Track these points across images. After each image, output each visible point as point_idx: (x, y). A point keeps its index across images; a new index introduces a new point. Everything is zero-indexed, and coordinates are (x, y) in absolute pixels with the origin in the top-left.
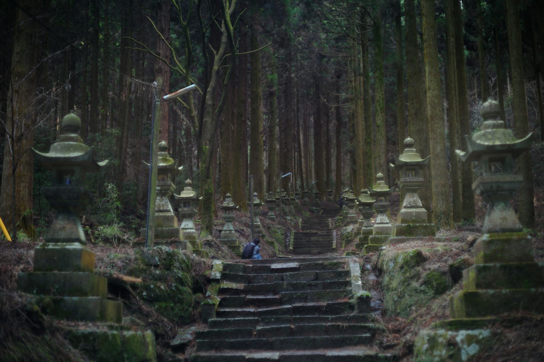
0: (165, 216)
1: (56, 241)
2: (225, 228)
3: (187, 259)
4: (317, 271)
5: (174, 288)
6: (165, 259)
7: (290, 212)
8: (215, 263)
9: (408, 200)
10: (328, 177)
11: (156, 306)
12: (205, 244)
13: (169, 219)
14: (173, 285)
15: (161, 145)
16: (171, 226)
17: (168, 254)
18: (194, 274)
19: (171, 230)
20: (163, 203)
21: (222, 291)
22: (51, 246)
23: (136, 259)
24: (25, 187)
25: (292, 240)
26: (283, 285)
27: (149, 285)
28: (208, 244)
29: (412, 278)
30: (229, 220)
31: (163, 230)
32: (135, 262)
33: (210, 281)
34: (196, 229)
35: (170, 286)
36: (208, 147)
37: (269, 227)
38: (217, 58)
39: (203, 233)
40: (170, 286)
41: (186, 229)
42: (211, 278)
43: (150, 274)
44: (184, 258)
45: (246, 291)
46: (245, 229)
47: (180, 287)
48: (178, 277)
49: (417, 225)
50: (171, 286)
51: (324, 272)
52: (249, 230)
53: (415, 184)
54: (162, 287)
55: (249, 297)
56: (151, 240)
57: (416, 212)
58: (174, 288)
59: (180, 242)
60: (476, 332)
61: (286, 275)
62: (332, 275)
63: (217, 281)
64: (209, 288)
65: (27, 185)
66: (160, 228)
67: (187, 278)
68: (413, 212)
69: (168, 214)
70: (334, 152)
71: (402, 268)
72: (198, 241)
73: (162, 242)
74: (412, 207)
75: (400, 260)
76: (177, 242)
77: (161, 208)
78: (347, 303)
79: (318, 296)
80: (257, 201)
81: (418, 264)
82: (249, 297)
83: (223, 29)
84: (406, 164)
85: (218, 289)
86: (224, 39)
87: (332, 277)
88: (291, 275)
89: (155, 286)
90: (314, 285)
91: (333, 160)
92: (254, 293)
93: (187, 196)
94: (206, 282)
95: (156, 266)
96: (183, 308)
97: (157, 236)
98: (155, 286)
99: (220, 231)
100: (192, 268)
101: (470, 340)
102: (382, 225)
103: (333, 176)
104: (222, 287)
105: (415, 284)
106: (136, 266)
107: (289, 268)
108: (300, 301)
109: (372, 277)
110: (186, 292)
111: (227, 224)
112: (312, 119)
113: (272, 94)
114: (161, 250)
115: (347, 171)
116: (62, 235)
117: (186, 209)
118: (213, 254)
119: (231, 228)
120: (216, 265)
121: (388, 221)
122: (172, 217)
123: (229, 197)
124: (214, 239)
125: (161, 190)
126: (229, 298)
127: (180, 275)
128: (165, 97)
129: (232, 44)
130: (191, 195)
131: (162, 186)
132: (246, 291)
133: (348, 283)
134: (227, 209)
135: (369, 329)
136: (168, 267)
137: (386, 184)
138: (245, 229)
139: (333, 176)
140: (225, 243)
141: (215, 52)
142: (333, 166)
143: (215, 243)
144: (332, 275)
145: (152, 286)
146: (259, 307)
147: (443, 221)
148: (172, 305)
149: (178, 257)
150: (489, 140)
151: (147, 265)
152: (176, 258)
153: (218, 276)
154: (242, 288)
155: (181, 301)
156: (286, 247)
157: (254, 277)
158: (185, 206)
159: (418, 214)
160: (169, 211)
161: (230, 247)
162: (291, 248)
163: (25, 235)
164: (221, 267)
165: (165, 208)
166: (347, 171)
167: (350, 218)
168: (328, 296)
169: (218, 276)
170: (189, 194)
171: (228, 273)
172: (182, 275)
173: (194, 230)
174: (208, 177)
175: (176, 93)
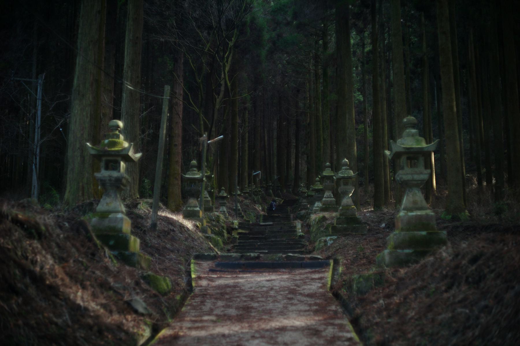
1: (191, 207)
9: (327, 194)
17: (218, 216)
21: (239, 234)
22: (189, 209)
29: (321, 227)
31: (117, 218)
33: (234, 229)
35: (219, 229)
36: (212, 158)
38: (218, 100)
45: (249, 234)
60: (333, 237)
63: (236, 229)
64: (233, 232)
70: (293, 151)
71: (317, 223)
75: (317, 220)
81: (324, 221)
83: (223, 82)
84: (326, 176)
86: (223, 88)
91: (293, 156)
95: (214, 221)
101: (331, 239)
103: (292, 172)
105: (322, 229)
109: (306, 229)
112: (275, 123)
113: (245, 109)
115: (303, 167)
116: (193, 205)
123: (223, 190)
133: (295, 231)
135: (302, 245)
139: (292, 172)
141: (216, 97)
142: (293, 162)
150: (343, 174)
153: (237, 227)
159: (331, 201)
166: (303, 167)
169: (237, 227)
171: (241, 226)
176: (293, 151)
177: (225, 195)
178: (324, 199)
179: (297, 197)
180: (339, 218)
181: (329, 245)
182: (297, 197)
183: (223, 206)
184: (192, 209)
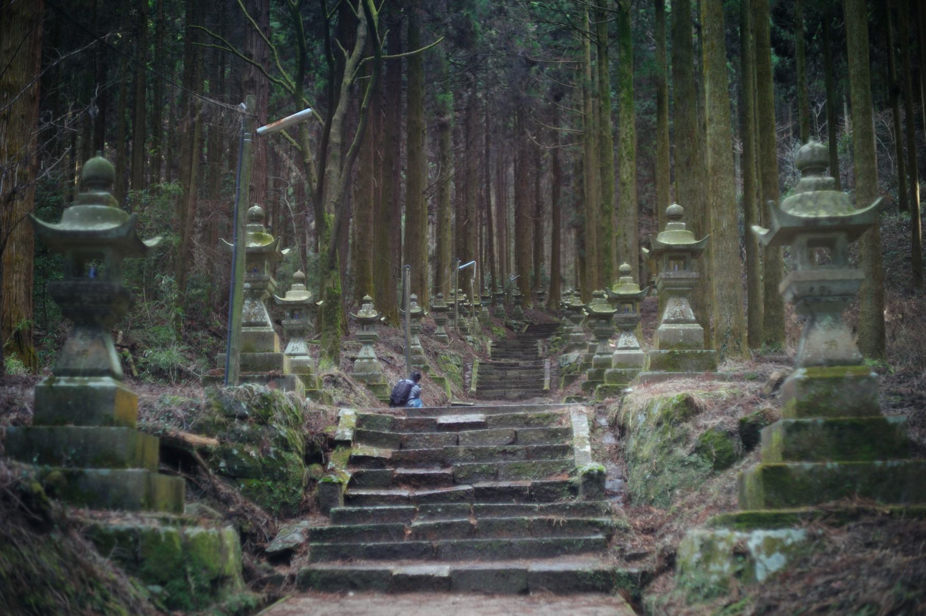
0: (259, 334)
1: (72, 373)
2: (362, 354)
3: (296, 405)
5: (272, 456)
6: (258, 407)
8: (343, 413)
11: (243, 486)
12: (328, 381)
13: (266, 338)
14: (272, 449)
15: (252, 211)
17: (264, 398)
19: (269, 356)
21: (355, 461)
22: (63, 382)
23: (209, 406)
25: (475, 376)
28: (333, 381)
29: (676, 441)
30: (368, 341)
31: (254, 357)
32: (207, 411)
33: (333, 443)
34: (312, 356)
37: (436, 354)
38: (349, 63)
39: (324, 363)
40: (265, 452)
41: (295, 355)
42: (336, 438)
43: (233, 431)
44: (291, 404)
45: (395, 462)
47: (284, 454)
48: (280, 436)
49: (687, 351)
50: (268, 452)
51: (528, 431)
55: (401, 471)
57: (684, 330)
58: (272, 456)
59: (284, 377)
60: (780, 534)
61: (463, 435)
62: (542, 435)
63: (347, 444)
64: (333, 455)
66: (249, 354)
69: (264, 330)
70: (548, 227)
71: (659, 424)
74: (677, 322)
75: (657, 412)
76: (278, 377)
77: (253, 320)
78: (565, 483)
79: (516, 470)
81: (686, 417)
82: (401, 471)
83: (360, 14)
84: (669, 249)
86: (362, 31)
87: (541, 438)
88: (472, 435)
89: (241, 451)
95: (243, 418)
97: (244, 367)
98: (241, 451)
99: (353, 359)
101: (771, 546)
102: (627, 352)
103: (546, 268)
104: (354, 454)
105: (681, 452)
106: (208, 418)
109: (609, 440)
110: (293, 463)
113: (443, 127)
114: (251, 390)
117: (294, 321)
118: (340, 398)
120: (345, 417)
123: (368, 301)
124: (343, 373)
125: (252, 289)
126: (366, 473)
127: (282, 434)
130: (304, 298)
131: (254, 282)
135: (602, 527)
138: (395, 355)
139: (546, 268)
140: (360, 379)
141: (346, 54)
142: (547, 250)
143: (344, 379)
144: (542, 435)
145: (235, 452)
146: (417, 488)
148: (269, 483)
150: (808, 209)
151: (227, 416)
152: (277, 404)
153: (349, 435)
154: (389, 456)
157: (409, 439)
158: (292, 316)
160: (265, 324)
161: (369, 387)
162: (473, 389)
163: (18, 362)
165: (258, 320)
167: (574, 339)
168: (534, 471)
169: (349, 435)
170: (300, 295)
173: (307, 358)
174: (332, 268)
176: (548, 227)
177: (373, 315)
178: (663, 327)
179: (556, 319)
180: (797, 427)
181: (761, 576)
182: (556, 319)
183: (366, 343)
184: (76, 382)
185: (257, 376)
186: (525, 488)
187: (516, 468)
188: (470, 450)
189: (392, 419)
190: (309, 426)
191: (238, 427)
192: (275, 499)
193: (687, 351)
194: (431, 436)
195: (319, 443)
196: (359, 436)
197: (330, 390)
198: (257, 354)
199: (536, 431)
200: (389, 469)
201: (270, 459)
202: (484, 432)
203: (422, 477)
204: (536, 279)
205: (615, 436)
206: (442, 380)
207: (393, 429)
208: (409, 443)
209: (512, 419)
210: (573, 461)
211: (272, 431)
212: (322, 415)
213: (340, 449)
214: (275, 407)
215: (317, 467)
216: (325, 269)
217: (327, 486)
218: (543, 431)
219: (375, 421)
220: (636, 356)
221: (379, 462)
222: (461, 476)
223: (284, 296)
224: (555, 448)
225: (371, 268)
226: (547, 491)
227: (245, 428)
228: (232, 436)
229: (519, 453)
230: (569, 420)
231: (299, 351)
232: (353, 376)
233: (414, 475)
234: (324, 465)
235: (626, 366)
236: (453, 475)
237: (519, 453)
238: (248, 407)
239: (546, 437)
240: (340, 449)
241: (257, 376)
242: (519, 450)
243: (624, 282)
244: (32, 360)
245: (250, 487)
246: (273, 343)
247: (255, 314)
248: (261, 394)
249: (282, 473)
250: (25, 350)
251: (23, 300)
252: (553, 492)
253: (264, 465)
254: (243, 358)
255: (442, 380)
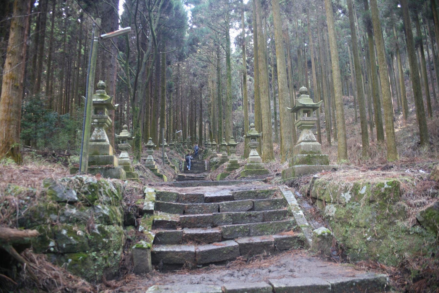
0: (102, 145)
2: (148, 158)
3: (117, 189)
4: (254, 200)
5: (97, 232)
6: (86, 193)
7: (179, 151)
8: (147, 191)
10: (195, 135)
11: (70, 260)
12: (136, 168)
13: (106, 148)
14: (96, 226)
15: (100, 84)
16: (106, 154)
17: (91, 186)
18: (125, 204)
19: (107, 157)
20: (100, 133)
21: (156, 225)
23: (43, 194)
24: (14, 128)
25: (183, 166)
26: (222, 217)
27: (60, 231)
28: (138, 168)
30: (151, 153)
31: (99, 158)
32: (42, 198)
33: (142, 213)
34: (131, 159)
37: (171, 159)
38: (145, 55)
39: (135, 161)
40: (90, 229)
41: (123, 158)
42: (144, 208)
43: (63, 215)
44: (113, 188)
46: (159, 159)
47: (106, 228)
48: (104, 214)
49: (315, 155)
50: (93, 229)
51: (260, 201)
52: (161, 160)
53: (310, 122)
54: (80, 233)
55: (187, 231)
56: (85, 167)
57: (312, 145)
58: (97, 232)
59: (114, 168)
61: (222, 205)
62: (268, 204)
63: (150, 212)
64: (141, 220)
65: (15, 127)
66: (96, 156)
67: (116, 213)
68: (310, 145)
69: (104, 143)
72: (131, 167)
73: (98, 168)
74: (309, 141)
76: (111, 168)
77: (98, 138)
78: (295, 237)
79: (261, 229)
80: (166, 144)
82: (187, 231)
85: (151, 221)
87: (268, 206)
88: (227, 204)
89: (70, 231)
90: (253, 216)
92: (191, 225)
93: (124, 136)
94: (138, 214)
95: (72, 203)
96: (109, 255)
97: (90, 163)
98: (70, 231)
99: (145, 160)
100: (123, 197)
102: (254, 157)
104: (155, 219)
106: (42, 205)
107: (223, 197)
108: (243, 236)
110: (113, 233)
111: (149, 156)
114: (81, 181)
117: (123, 144)
118: (141, 174)
119: (152, 158)
120: (149, 193)
121: (258, 155)
122: (108, 146)
124: (142, 165)
125: (98, 123)
126: (165, 233)
127: (105, 212)
128: (102, 36)
129: (155, 44)
130: (127, 135)
131: (99, 119)
132: (183, 224)
134: (150, 147)
136: (90, 203)
137: (256, 130)
138: (159, 159)
140: (148, 167)
141: (144, 52)
143: (142, 167)
144: (268, 204)
145: (64, 232)
146: (199, 243)
147: (289, 154)
148: (94, 254)
149: (104, 188)
151: (59, 202)
152: (102, 190)
153: (151, 206)
154: (178, 220)
155: (106, 247)
156: (180, 169)
157: (189, 207)
158: (123, 143)
160: (104, 141)
161: (151, 170)
162: (183, 170)
163: (12, 160)
164: (154, 196)
165: (101, 138)
167: (213, 154)
168: (272, 229)
169: (151, 206)
170: (125, 134)
172: (110, 212)
173: (128, 159)
174: (138, 127)
175: (112, 33)
177: (152, 144)
185: (99, 168)
186: (271, 243)
187: (261, 227)
188: (230, 215)
189: (177, 194)
190: (126, 200)
191: (68, 211)
192: (98, 265)
193: (315, 155)
194: (202, 205)
195: (133, 212)
196: (158, 207)
197: (136, 172)
198: (100, 156)
199: (265, 201)
200: (179, 230)
201: (94, 234)
202: (235, 203)
203: (201, 235)
204: (195, 138)
205: (309, 203)
206: (174, 167)
207: (177, 201)
208: (189, 210)
209: (248, 193)
210: (295, 220)
211: (98, 211)
212: (134, 191)
213: (147, 216)
214: (100, 192)
215: (131, 229)
216: (136, 127)
217: (139, 250)
218: (269, 201)
219: (167, 195)
220: (258, 158)
221: (172, 225)
222: (227, 234)
223: (119, 134)
224: (280, 212)
225: (149, 131)
226: (284, 243)
227: (74, 211)
228: (63, 219)
229: (259, 216)
230: (281, 194)
231: (125, 157)
232: (145, 166)
233: (196, 235)
234: (137, 227)
235: (254, 162)
236: (222, 233)
237: (259, 216)
238: (78, 193)
239: (271, 204)
240: (147, 216)
241: (99, 168)
242: (259, 214)
243: (252, 130)
244: (19, 159)
245: (77, 261)
246: (109, 150)
247: (100, 136)
248: (89, 183)
249: (104, 243)
250: (16, 156)
251: (15, 135)
252: (288, 244)
253: (89, 241)
254: (91, 157)
255: (174, 167)
